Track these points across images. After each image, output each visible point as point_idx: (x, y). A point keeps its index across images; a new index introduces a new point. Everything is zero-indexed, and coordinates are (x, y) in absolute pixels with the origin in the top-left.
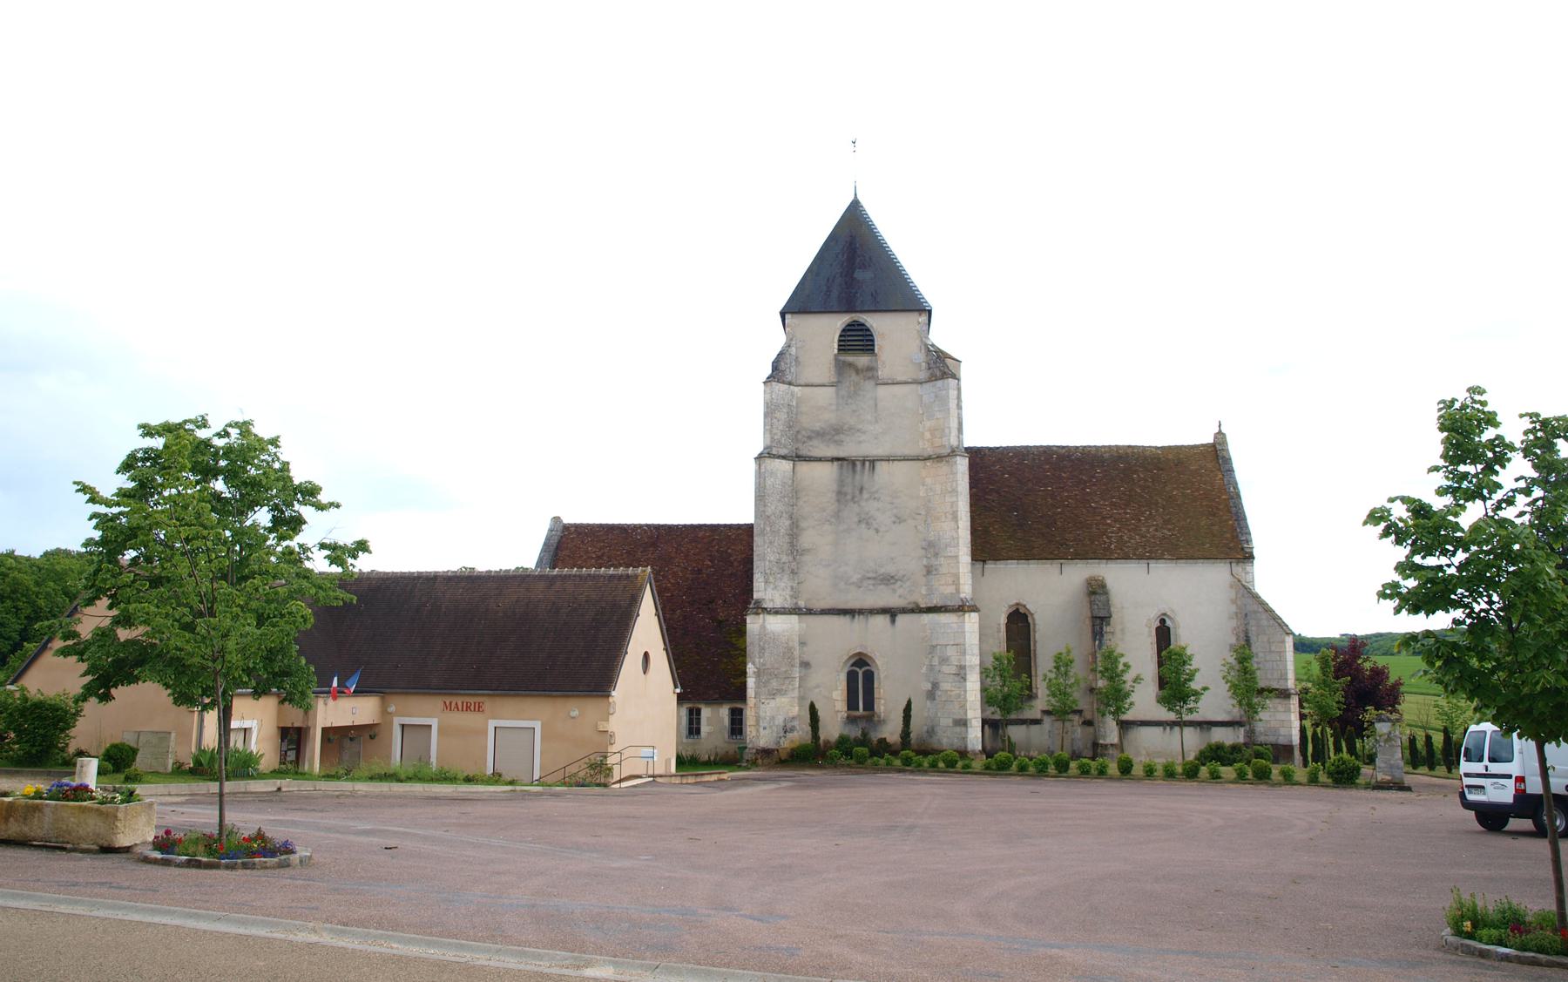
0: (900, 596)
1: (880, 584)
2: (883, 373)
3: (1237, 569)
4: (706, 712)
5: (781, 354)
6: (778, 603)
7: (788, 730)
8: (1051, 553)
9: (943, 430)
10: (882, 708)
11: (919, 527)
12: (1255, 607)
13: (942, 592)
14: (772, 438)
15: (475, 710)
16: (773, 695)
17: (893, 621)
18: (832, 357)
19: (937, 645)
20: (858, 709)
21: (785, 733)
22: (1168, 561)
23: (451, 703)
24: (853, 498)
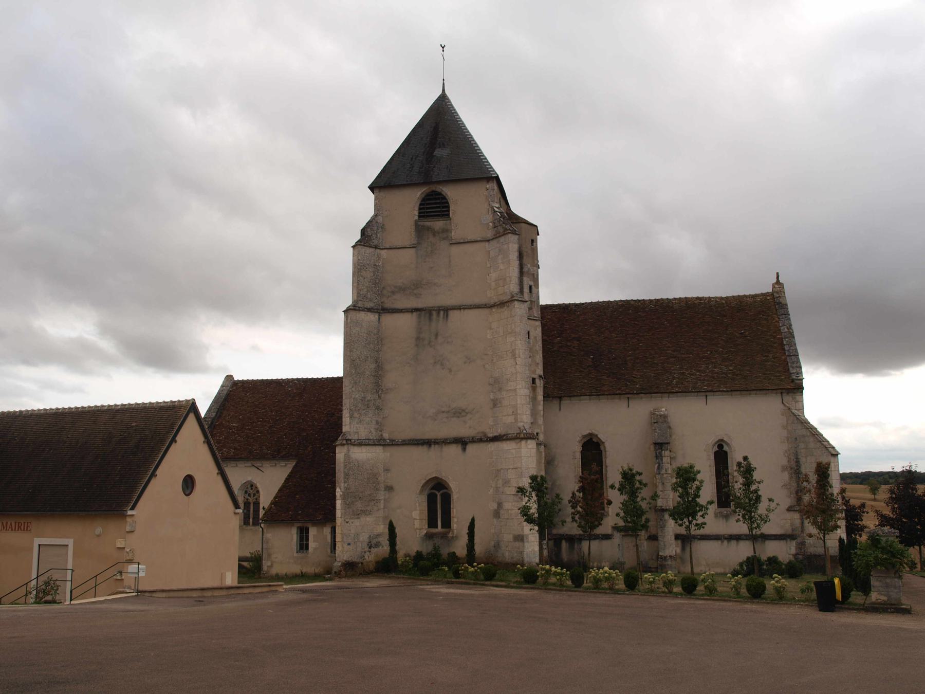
0: (470, 427)
1: (453, 417)
2: (456, 234)
3: (788, 398)
4: (313, 532)
5: (369, 224)
6: (363, 434)
7: (373, 545)
8: (619, 389)
9: (505, 279)
10: (455, 525)
11: (487, 366)
12: (804, 432)
13: (505, 422)
14: (358, 293)
15: (15, 530)
16: (357, 515)
17: (464, 449)
18: (413, 223)
19: (501, 469)
20: (437, 527)
21: (370, 548)
22: (724, 393)
23: (7, 523)
24: (430, 342)
